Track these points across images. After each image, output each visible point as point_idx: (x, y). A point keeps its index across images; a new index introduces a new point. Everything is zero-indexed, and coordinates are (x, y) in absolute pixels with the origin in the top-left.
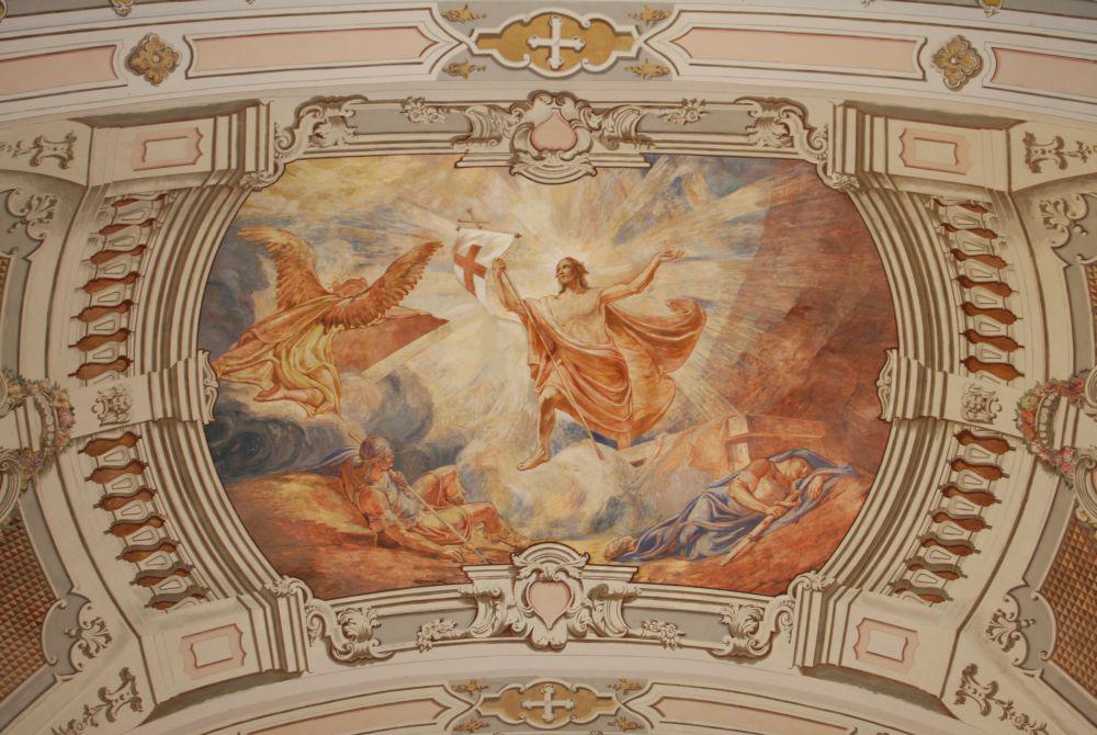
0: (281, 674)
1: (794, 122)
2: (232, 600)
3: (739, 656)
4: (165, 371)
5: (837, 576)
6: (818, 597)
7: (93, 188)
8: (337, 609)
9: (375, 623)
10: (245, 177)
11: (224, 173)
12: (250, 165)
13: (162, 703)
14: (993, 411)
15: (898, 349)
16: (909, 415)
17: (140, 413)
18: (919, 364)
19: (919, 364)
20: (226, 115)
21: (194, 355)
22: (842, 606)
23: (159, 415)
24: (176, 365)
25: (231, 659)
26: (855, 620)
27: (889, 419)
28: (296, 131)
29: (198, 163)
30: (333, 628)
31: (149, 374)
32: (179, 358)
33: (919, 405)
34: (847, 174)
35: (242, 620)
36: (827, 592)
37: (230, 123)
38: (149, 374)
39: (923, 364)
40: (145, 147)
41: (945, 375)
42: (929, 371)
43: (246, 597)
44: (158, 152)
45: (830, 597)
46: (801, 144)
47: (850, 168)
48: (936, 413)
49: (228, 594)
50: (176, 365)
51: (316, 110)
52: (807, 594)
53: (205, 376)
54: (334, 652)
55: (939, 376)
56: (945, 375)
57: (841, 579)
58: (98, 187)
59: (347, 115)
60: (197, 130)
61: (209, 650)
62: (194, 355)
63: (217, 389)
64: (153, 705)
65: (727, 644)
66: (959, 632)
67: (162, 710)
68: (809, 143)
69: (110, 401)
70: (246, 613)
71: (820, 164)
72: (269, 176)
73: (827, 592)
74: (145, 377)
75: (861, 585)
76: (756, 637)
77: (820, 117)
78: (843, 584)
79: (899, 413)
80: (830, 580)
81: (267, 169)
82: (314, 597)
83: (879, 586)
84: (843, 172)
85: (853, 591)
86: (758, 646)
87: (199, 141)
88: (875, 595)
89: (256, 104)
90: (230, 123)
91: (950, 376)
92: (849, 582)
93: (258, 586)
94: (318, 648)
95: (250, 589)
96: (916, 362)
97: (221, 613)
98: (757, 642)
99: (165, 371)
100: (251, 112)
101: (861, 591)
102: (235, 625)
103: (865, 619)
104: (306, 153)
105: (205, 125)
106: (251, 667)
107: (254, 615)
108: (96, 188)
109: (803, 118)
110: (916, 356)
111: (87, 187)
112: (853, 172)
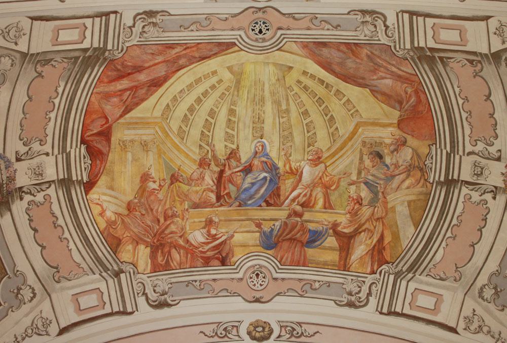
0: (124, 313)
1: (380, 23)
2: (97, 276)
3: (350, 305)
4: (64, 154)
5: (402, 267)
6: (392, 277)
7: (31, 54)
8: (151, 279)
9: (170, 286)
10: (107, 52)
11: (95, 49)
12: (110, 47)
13: (63, 328)
14: (486, 174)
15: (436, 144)
16: (442, 179)
17: (51, 173)
18: (447, 151)
19: (447, 151)
20: (99, 17)
21: (79, 146)
22: (404, 283)
23: (61, 177)
24: (70, 151)
25: (98, 306)
26: (410, 290)
27: (431, 182)
28: (133, 29)
29: (84, 43)
30: (149, 291)
31: (56, 156)
32: (71, 148)
33: (447, 174)
34: (407, 49)
35: (103, 286)
36: (398, 275)
37: (101, 21)
38: (56, 156)
39: (449, 152)
40: (58, 33)
41: (461, 157)
42: (452, 155)
43: (104, 274)
44: (64, 36)
45: (399, 277)
46: (148, 285)
47: (408, 46)
48: (455, 177)
49: (95, 273)
50: (70, 151)
51: (144, 18)
52: (387, 275)
53: (84, 158)
54: (150, 301)
55: (457, 157)
56: (461, 157)
57: (404, 269)
58: (34, 54)
59: (158, 21)
60: (84, 24)
61: (86, 302)
62: (79, 146)
63: (91, 165)
64: (59, 330)
65: (345, 299)
66: (465, 294)
67: (62, 331)
68: (144, 285)
69: (35, 169)
70: (105, 282)
71: (392, 45)
72: (119, 53)
73: (398, 275)
74: (54, 157)
75: (415, 273)
76: (360, 295)
77: (391, 20)
78: (406, 271)
79: (437, 178)
80: (399, 268)
81: (118, 49)
82: (391, 46)
83: (419, 270)
84: (405, 49)
85: (410, 275)
86: (361, 300)
87: (85, 30)
88: (421, 277)
89: (115, 12)
90: (101, 21)
91: (463, 157)
92: (409, 270)
93: (110, 268)
94: (141, 300)
95: (106, 269)
96: (445, 151)
97: (92, 282)
98: (360, 298)
99: (64, 154)
100: (112, 16)
101: (415, 275)
102: (99, 288)
103: (416, 289)
104: (138, 41)
105: (88, 22)
106: (108, 310)
107: (108, 283)
108: (32, 55)
109: (384, 22)
110: (445, 148)
111: (28, 54)
112: (410, 48)
